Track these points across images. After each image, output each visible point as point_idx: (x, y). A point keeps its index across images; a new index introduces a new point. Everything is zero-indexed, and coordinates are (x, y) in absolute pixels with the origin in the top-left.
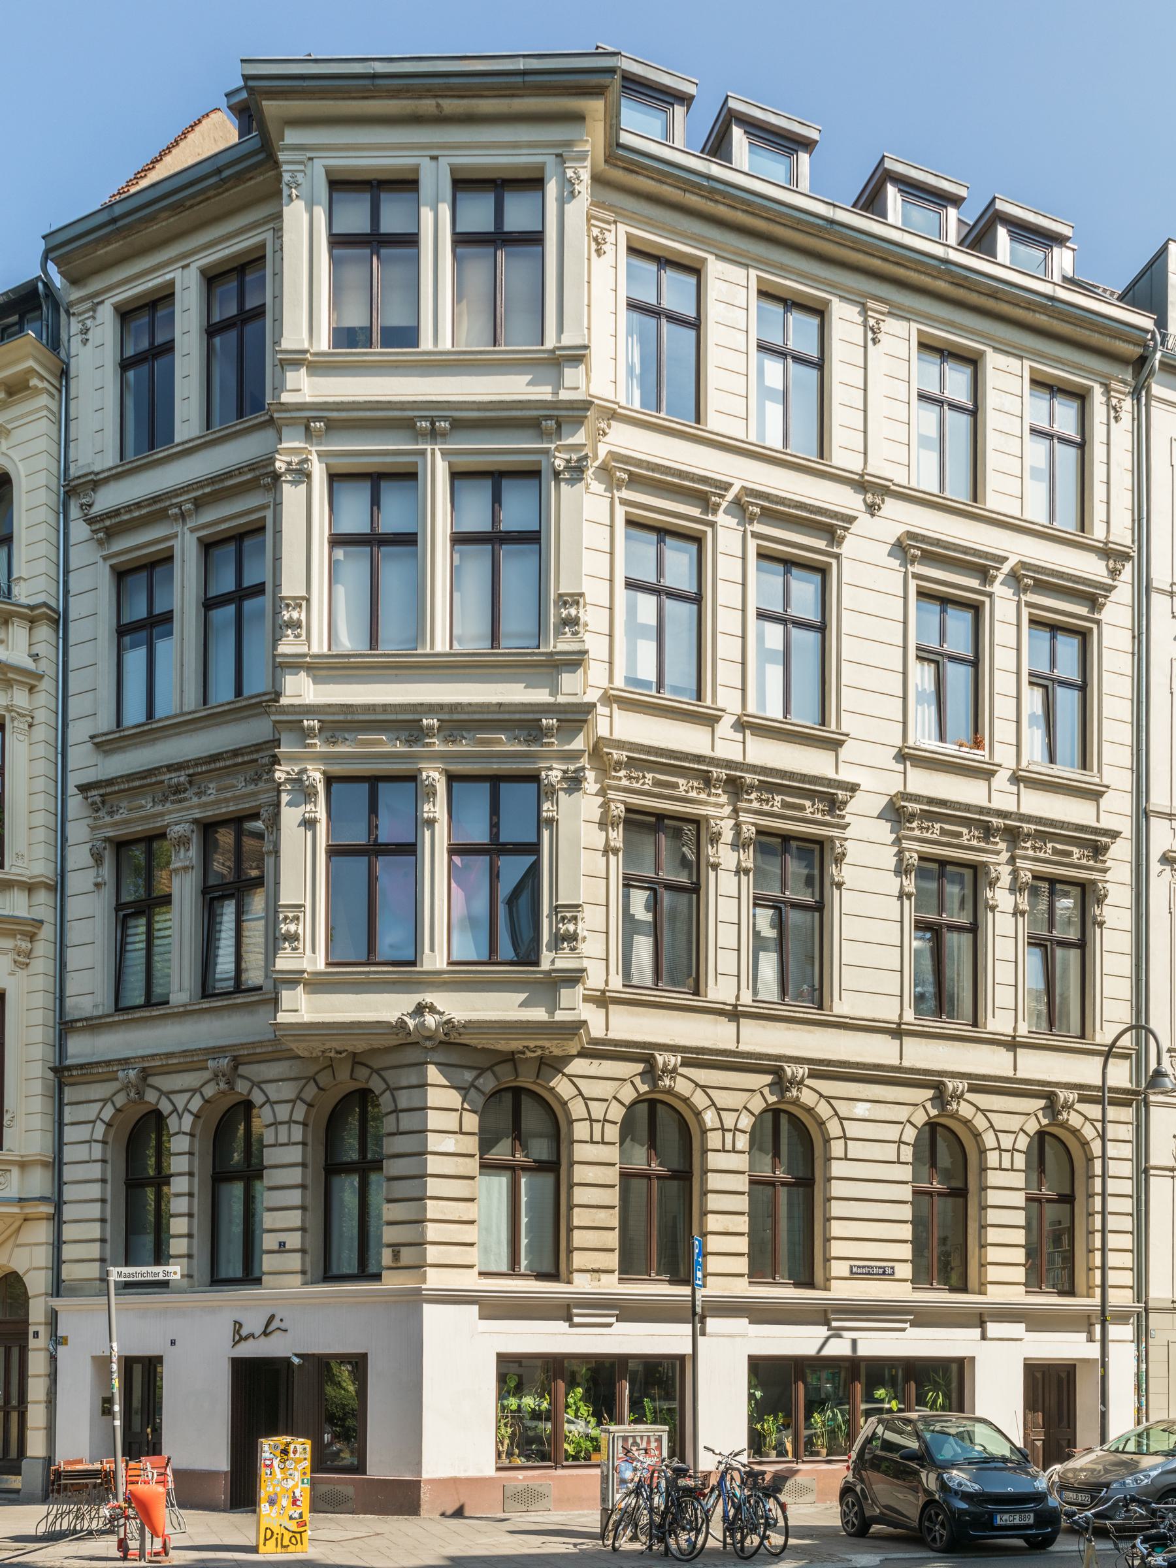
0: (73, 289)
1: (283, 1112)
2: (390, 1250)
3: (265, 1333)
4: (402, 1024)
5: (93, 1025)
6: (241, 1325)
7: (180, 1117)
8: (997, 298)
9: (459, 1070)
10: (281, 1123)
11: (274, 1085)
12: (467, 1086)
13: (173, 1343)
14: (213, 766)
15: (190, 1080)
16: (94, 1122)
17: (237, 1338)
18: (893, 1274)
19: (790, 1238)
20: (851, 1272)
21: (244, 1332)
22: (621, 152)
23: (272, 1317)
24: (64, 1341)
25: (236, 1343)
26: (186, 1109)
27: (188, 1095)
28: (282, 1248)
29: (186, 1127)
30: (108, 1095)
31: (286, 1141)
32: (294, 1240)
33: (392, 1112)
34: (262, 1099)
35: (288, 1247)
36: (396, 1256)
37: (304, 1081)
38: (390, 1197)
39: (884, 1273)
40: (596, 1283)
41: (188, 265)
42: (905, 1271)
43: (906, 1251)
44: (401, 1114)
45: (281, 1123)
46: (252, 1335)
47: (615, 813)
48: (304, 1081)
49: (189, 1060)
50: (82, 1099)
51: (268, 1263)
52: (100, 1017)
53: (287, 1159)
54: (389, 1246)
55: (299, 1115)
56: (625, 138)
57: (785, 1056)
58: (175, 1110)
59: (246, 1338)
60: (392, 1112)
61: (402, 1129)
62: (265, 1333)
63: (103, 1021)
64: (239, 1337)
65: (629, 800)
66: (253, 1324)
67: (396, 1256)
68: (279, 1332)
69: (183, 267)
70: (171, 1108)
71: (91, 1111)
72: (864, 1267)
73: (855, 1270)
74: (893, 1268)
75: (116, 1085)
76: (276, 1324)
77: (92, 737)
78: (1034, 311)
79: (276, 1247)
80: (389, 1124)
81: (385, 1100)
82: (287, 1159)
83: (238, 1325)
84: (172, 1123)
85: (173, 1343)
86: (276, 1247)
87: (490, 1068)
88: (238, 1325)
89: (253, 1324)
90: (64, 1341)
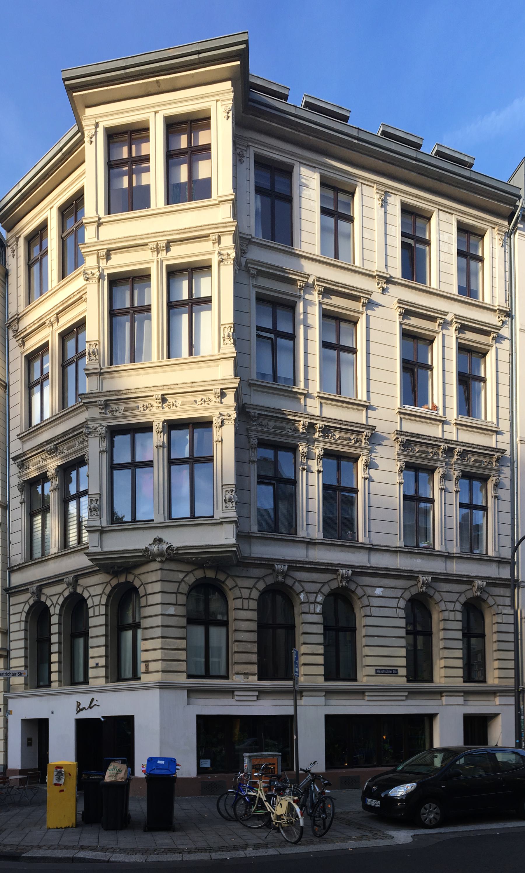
0: (9, 234)
1: (96, 600)
2: (144, 664)
3: (90, 707)
4: (146, 550)
5: (21, 568)
6: (80, 704)
7: (55, 607)
8: (441, 181)
9: (177, 573)
10: (96, 606)
11: (93, 588)
12: (180, 581)
13: (52, 712)
14: (65, 438)
15: (59, 589)
16: (21, 612)
17: (78, 709)
18: (397, 673)
19: (340, 665)
20: (376, 673)
21: (81, 707)
22: (251, 103)
23: (93, 699)
24: (10, 713)
25: (78, 712)
26: (57, 603)
27: (58, 596)
28: (97, 666)
29: (57, 612)
30: (26, 600)
31: (98, 614)
32: (102, 662)
33: (144, 596)
34: (88, 595)
35: (99, 665)
36: (147, 667)
37: (105, 584)
38: (144, 638)
39: (392, 673)
40: (247, 680)
41: (52, 207)
42: (403, 672)
43: (403, 662)
44: (148, 596)
45: (96, 606)
46: (84, 708)
47: (253, 443)
48: (105, 584)
49: (56, 580)
50: (17, 603)
51: (91, 673)
52: (23, 563)
53: (97, 622)
54: (144, 662)
55: (104, 601)
56: (252, 80)
57: (340, 564)
58: (53, 604)
59: (82, 710)
60: (144, 596)
61: (149, 604)
62: (90, 707)
63: (24, 565)
64: (79, 710)
65: (260, 437)
66: (85, 704)
67: (147, 667)
68: (96, 706)
69: (51, 208)
70: (51, 603)
71: (19, 608)
72: (382, 670)
73: (378, 671)
74: (397, 670)
75: (29, 595)
76: (94, 702)
77: (18, 436)
78: (460, 188)
79: (95, 665)
80: (143, 602)
81: (141, 591)
82: (97, 622)
83: (79, 704)
84: (52, 610)
85: (52, 712)
86: (95, 665)
87: (191, 572)
88: (79, 704)
89: (85, 704)
90: (10, 713)
